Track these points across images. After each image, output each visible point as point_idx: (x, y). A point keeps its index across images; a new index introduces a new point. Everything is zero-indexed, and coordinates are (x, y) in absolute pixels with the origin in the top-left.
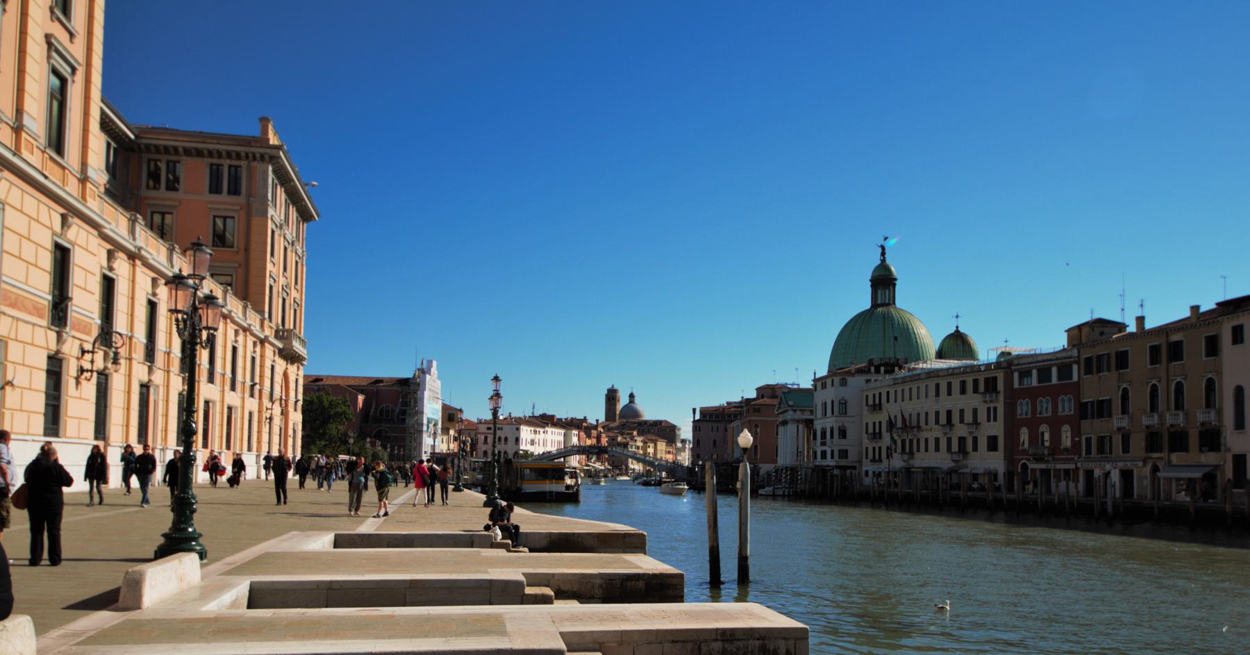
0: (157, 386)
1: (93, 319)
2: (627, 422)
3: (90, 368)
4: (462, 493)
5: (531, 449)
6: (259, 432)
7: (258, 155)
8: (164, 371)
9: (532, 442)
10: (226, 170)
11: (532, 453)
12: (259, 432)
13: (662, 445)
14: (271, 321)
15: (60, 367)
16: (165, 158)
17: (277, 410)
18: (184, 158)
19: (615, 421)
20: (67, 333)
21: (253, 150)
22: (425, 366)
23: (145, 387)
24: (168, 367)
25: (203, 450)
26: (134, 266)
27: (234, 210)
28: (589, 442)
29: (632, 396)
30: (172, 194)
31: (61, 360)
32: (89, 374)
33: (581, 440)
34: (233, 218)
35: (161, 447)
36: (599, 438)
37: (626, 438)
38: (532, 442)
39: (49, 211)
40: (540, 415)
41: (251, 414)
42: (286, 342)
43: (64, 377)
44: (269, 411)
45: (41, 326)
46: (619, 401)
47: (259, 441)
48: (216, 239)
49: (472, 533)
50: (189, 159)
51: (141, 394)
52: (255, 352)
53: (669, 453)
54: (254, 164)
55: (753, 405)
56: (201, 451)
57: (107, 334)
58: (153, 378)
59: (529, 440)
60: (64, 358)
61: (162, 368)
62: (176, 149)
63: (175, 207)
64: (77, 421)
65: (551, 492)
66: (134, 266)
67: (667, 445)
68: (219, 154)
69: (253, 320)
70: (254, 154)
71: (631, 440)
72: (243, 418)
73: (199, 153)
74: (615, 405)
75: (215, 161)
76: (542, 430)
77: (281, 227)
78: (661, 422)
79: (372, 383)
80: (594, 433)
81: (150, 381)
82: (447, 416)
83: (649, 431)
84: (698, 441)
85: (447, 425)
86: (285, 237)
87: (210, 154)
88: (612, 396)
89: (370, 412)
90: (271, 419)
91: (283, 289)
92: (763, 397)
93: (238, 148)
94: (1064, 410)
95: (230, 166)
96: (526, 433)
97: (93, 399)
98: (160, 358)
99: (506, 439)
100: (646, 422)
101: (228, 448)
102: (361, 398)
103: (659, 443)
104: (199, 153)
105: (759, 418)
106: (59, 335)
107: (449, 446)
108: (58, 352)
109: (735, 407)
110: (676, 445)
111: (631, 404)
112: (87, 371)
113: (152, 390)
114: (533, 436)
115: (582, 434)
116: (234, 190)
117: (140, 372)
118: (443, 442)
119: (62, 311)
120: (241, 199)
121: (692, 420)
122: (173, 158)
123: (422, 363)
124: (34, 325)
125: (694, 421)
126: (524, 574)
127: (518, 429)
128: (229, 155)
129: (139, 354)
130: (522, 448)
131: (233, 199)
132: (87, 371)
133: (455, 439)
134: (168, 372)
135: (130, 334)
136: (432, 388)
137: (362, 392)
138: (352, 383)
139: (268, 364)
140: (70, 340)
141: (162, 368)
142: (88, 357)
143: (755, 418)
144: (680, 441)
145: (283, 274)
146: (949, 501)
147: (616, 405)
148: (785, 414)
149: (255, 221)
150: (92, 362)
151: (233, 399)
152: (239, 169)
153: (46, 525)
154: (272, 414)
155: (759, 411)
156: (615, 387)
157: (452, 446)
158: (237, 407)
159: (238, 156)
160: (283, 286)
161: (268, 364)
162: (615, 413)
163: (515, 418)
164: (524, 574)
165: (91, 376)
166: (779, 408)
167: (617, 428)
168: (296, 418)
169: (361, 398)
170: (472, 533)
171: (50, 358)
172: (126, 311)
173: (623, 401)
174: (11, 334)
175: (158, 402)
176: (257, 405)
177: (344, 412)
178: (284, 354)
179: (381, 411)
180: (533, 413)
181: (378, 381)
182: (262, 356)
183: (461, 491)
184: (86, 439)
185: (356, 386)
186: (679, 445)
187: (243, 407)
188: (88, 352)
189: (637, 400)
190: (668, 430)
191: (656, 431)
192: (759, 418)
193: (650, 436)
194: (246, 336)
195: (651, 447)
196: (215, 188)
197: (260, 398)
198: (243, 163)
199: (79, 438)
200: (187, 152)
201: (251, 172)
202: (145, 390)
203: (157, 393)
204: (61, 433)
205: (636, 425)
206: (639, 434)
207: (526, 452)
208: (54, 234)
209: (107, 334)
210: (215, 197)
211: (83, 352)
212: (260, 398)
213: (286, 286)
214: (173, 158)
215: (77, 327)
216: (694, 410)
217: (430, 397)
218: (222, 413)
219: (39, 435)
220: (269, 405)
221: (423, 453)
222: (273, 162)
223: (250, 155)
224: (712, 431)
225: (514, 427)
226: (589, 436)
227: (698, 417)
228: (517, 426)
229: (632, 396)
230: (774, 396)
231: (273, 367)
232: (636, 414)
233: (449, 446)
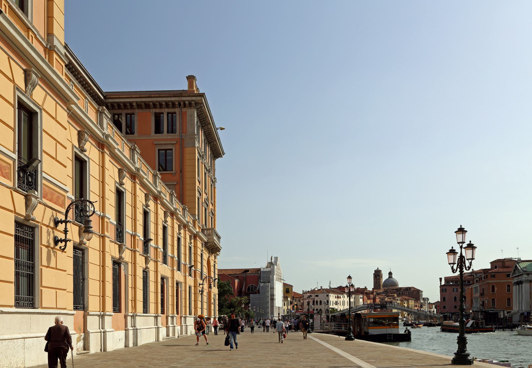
0: (127, 263)
1: (67, 192)
2: (388, 289)
3: (63, 238)
4: (354, 341)
5: (336, 307)
6: (195, 301)
7: (187, 103)
8: (132, 250)
9: (336, 303)
11: (337, 309)
12: (195, 301)
13: (412, 303)
14: (199, 222)
15: (33, 236)
16: (124, 112)
17: (206, 286)
18: (137, 110)
19: (380, 288)
20: (36, 198)
22: (273, 261)
23: (117, 263)
24: (135, 247)
25: (162, 315)
26: (103, 153)
27: (173, 144)
28: (369, 302)
29: (390, 273)
31: (33, 229)
32: (64, 243)
33: (365, 301)
34: (172, 150)
35: (132, 314)
36: (374, 299)
37: (390, 299)
38: (336, 303)
39: (8, 58)
40: (338, 287)
41: (190, 287)
42: (209, 237)
43: (37, 246)
44: (201, 286)
46: (382, 277)
47: (196, 308)
48: (160, 167)
50: (140, 111)
51: (114, 270)
52: (191, 243)
53: (416, 306)
54: (184, 110)
55: (490, 273)
56: (160, 316)
57: (81, 210)
58: (123, 256)
59: (334, 302)
60: (37, 226)
61: (130, 248)
62: (131, 104)
64: (54, 291)
65: (390, 334)
66: (103, 153)
67: (415, 302)
68: (161, 106)
69: (188, 219)
70: (184, 102)
71: (394, 299)
72: (186, 291)
73: (147, 106)
74: (380, 279)
75: (158, 111)
76: (341, 296)
77: (203, 158)
78: (410, 288)
79: (243, 272)
80: (372, 296)
81: (121, 258)
82: (285, 290)
83: (403, 294)
84: (444, 298)
85: (286, 295)
86: (205, 165)
88: (377, 274)
89: (242, 289)
90: (202, 291)
91: (205, 201)
92: (496, 267)
93: (173, 99)
95: (168, 113)
96: (332, 298)
97: (71, 271)
98: (128, 239)
99: (321, 302)
100: (401, 289)
101: (178, 313)
102: (236, 281)
103: (410, 301)
104: (147, 106)
105: (495, 281)
106: (27, 199)
107: (288, 307)
108: (27, 218)
109: (469, 276)
110: (420, 301)
111: (390, 279)
112: (61, 241)
113: (122, 267)
114: (335, 300)
115: (365, 297)
116: (172, 130)
117: (112, 250)
118: (284, 305)
119: (31, 175)
120: (176, 136)
121: (440, 285)
122: (130, 111)
123: (271, 259)
125: (441, 286)
127: (327, 296)
128: (167, 105)
129: (111, 233)
130: (330, 307)
131: (171, 136)
132: (61, 241)
133: (291, 303)
134: (135, 252)
135: (102, 214)
136: (278, 274)
137: (237, 277)
138: (231, 273)
139: (199, 252)
140: (40, 207)
141: (130, 248)
142: (61, 227)
143: (492, 281)
144: (422, 299)
145: (205, 191)
146: (227, 320)
147: (380, 279)
148: (520, 277)
149: (187, 150)
150: (66, 232)
151: (179, 276)
152: (174, 115)
153: (59, 360)
154: (203, 288)
155: (494, 276)
156: (380, 269)
157: (289, 307)
158: (181, 283)
159: (174, 105)
160: (205, 199)
161: (199, 252)
162: (380, 284)
163: (324, 289)
165: (65, 246)
166: (513, 274)
167: (383, 293)
168: (215, 290)
169: (236, 281)
171: (18, 224)
172: (97, 177)
173: (385, 277)
175: (128, 276)
176: (193, 282)
177: (228, 290)
178: (207, 246)
179: (249, 288)
180: (330, 286)
181: (246, 271)
182: (195, 247)
183: (352, 340)
184: (65, 309)
185: (233, 274)
186: (422, 301)
187: (185, 283)
188: (61, 222)
189: (393, 276)
190: (415, 293)
191: (407, 293)
192: (495, 281)
193: (404, 297)
194: (185, 231)
195: (406, 303)
196: (158, 130)
197: (195, 276)
198: (177, 110)
199: (57, 308)
200: (139, 106)
201: (183, 115)
202: (117, 267)
203: (126, 269)
204: (37, 304)
205: (395, 291)
206: (398, 296)
207: (333, 309)
208: (17, 88)
209: (81, 210)
210: (159, 136)
211: (57, 223)
212: (195, 276)
213: (206, 199)
214: (130, 111)
215: (49, 196)
216: (441, 279)
217: (277, 278)
218: (173, 287)
219: (11, 306)
220: (201, 282)
222: (198, 107)
223: (182, 103)
224: (454, 291)
225: (326, 295)
226: (369, 298)
227: (443, 283)
228: (327, 294)
229: (390, 273)
230: (504, 267)
232: (395, 284)
233: (288, 307)
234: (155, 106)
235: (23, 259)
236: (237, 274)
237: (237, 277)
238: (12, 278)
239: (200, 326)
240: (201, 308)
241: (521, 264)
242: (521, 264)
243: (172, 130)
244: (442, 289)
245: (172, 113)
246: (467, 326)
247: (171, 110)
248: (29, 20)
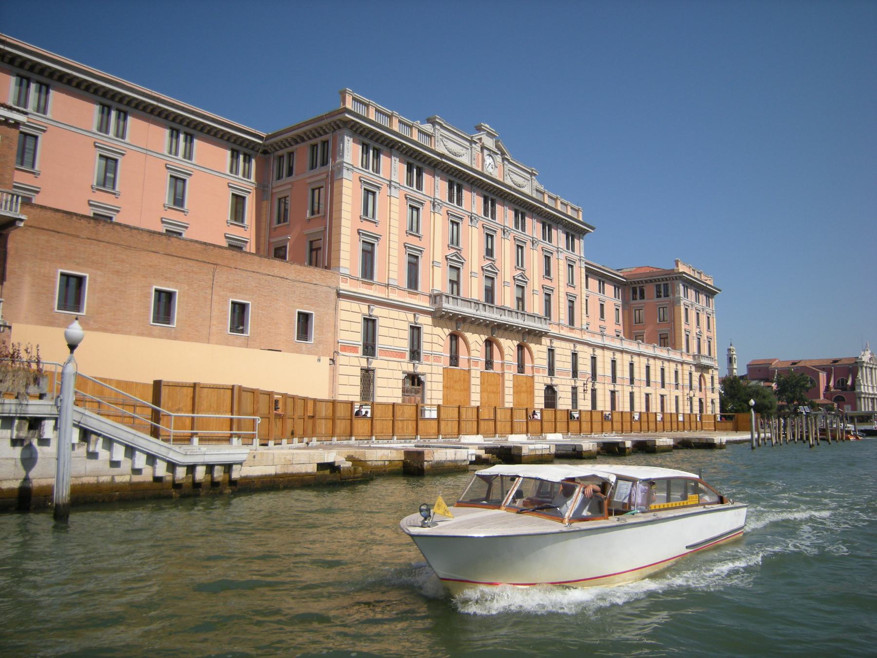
10: (662, 286)
21: (672, 276)
30: (642, 301)
45: (345, 268)
49: (155, 103)
54: (673, 281)
63: (643, 307)
64: (482, 423)
73: (651, 281)
87: (655, 280)
94: (865, 409)
122: (641, 285)
124: (349, 356)
126: (349, 458)
128: (663, 280)
131: (666, 299)
137: (823, 369)
164: (349, 458)
170: (155, 103)
174: (625, 375)
196: (659, 296)
198: (669, 282)
210: (659, 299)
221: (137, 479)
231: (323, 619)
234: (656, 281)
235: (574, 398)
236: (824, 366)
237: (824, 369)
238: (571, 404)
239: (522, 387)
240: (57, 459)
241: (505, 249)
242: (505, 249)
243: (667, 295)
244: (457, 245)
245: (667, 284)
246: (699, 484)
247: (665, 282)
248: (581, 494)
